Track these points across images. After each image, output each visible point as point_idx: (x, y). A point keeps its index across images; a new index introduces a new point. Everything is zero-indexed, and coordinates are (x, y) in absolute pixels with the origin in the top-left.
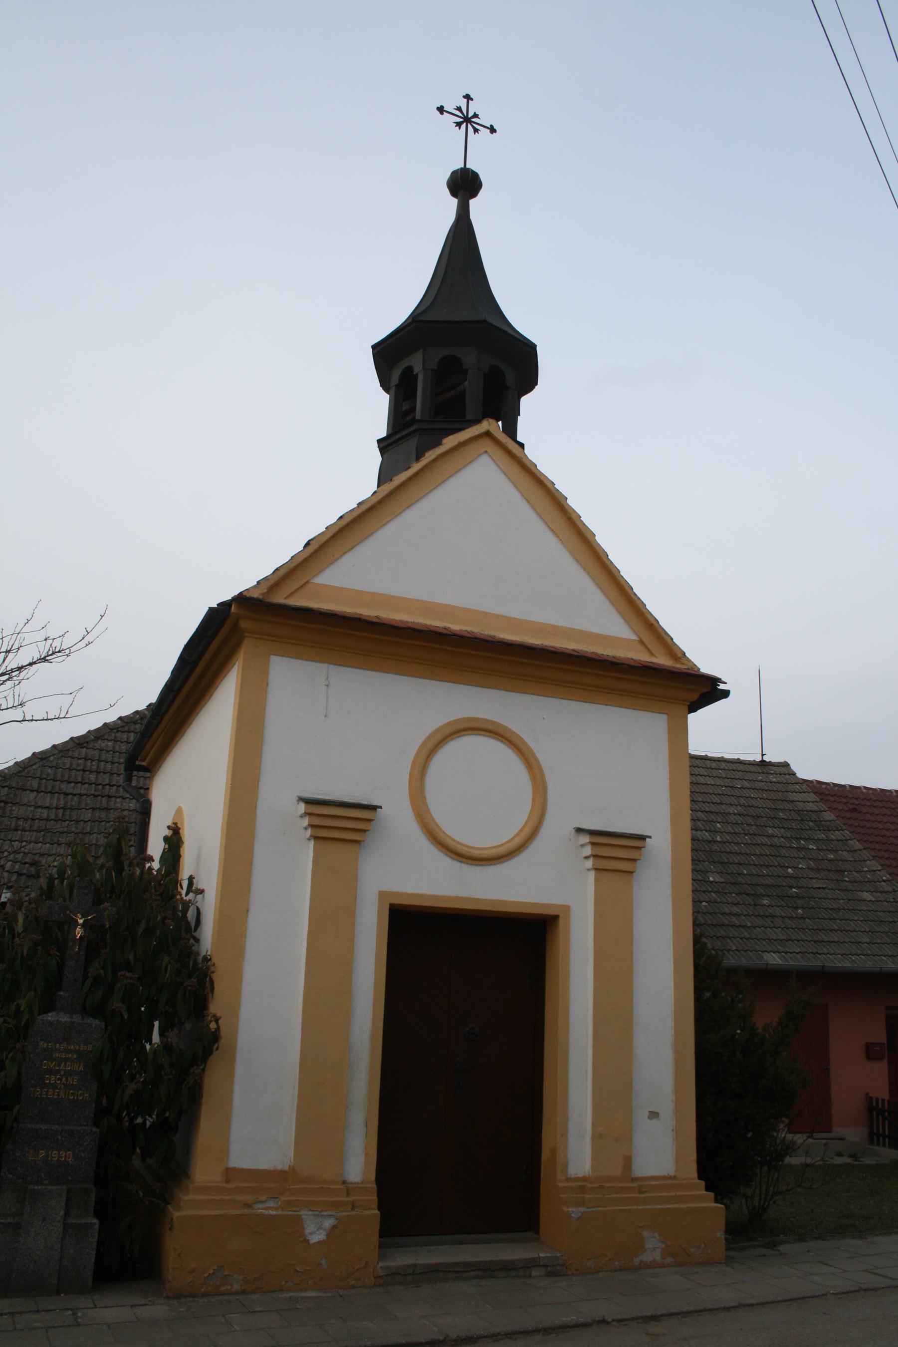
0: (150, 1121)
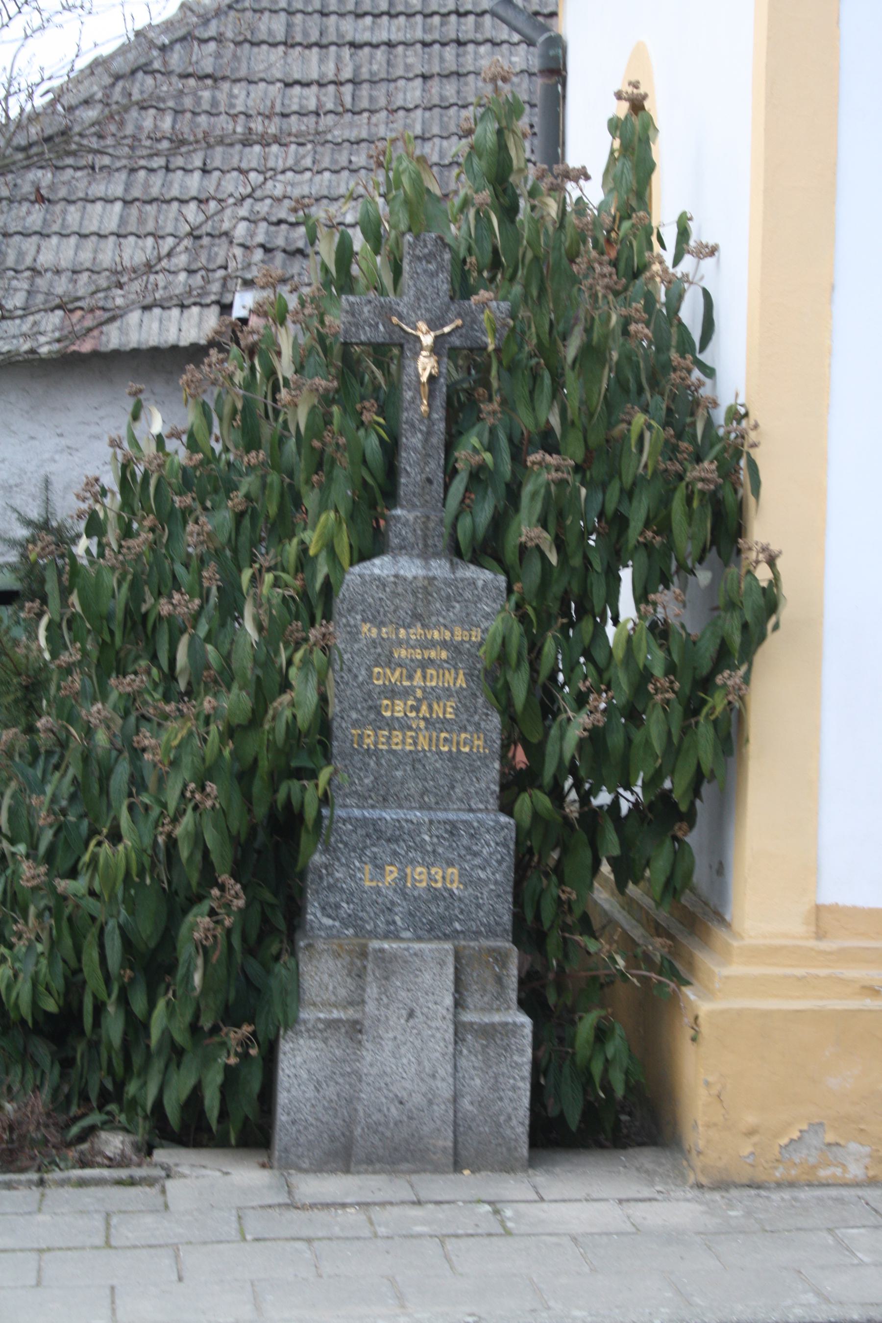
0: (628, 800)
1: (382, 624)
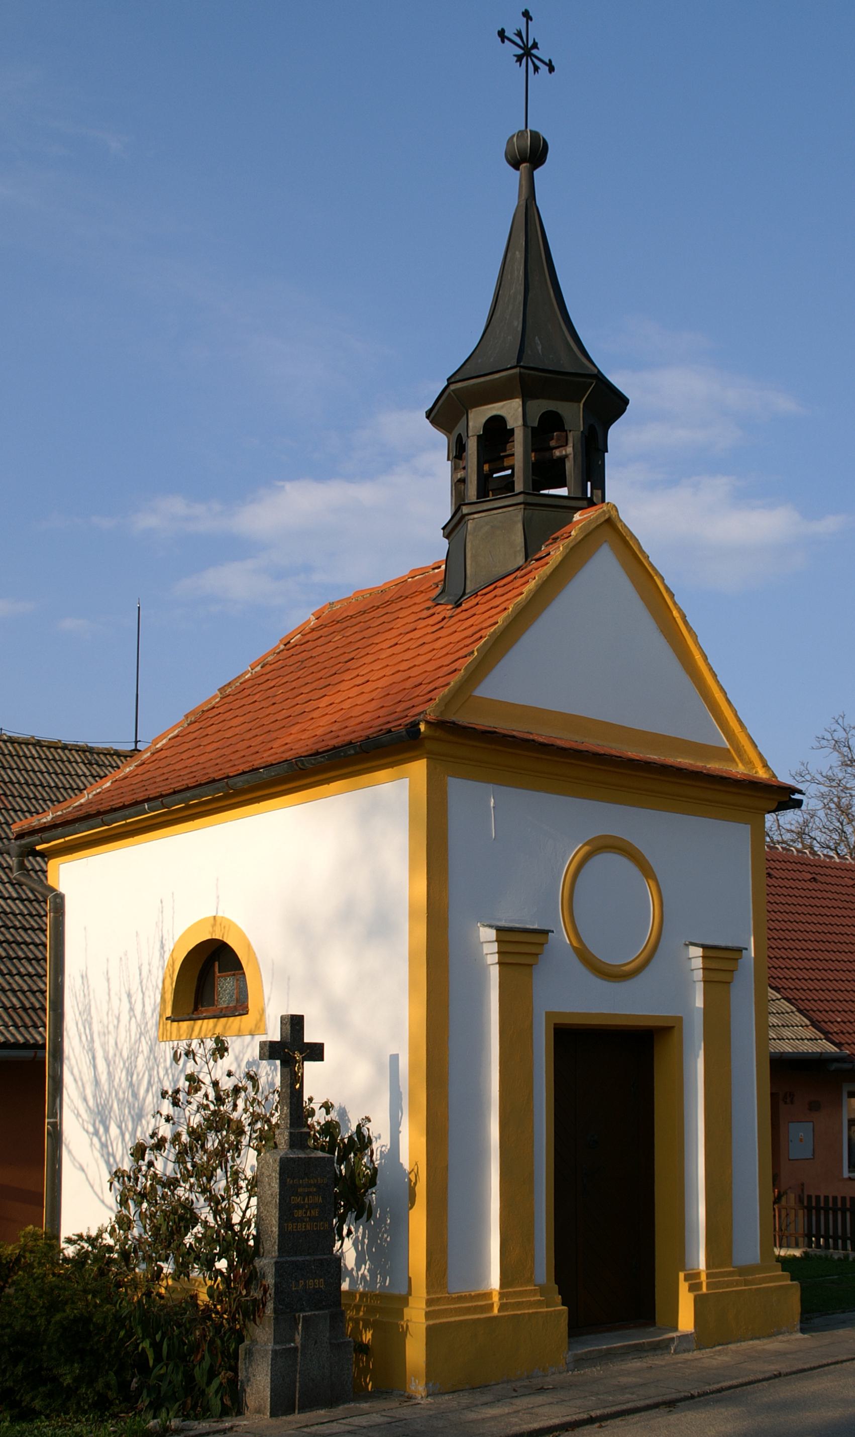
1: (294, 1178)
